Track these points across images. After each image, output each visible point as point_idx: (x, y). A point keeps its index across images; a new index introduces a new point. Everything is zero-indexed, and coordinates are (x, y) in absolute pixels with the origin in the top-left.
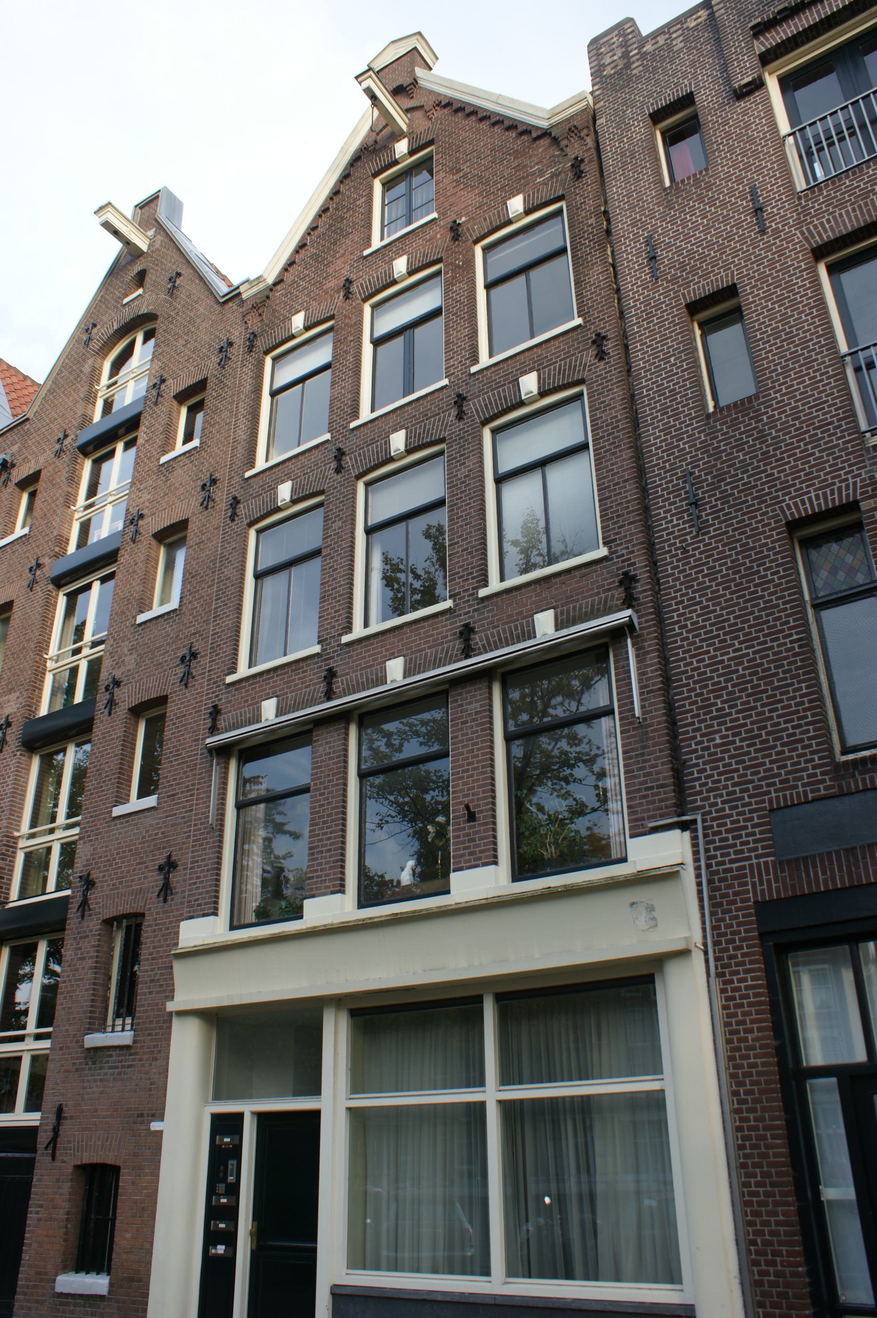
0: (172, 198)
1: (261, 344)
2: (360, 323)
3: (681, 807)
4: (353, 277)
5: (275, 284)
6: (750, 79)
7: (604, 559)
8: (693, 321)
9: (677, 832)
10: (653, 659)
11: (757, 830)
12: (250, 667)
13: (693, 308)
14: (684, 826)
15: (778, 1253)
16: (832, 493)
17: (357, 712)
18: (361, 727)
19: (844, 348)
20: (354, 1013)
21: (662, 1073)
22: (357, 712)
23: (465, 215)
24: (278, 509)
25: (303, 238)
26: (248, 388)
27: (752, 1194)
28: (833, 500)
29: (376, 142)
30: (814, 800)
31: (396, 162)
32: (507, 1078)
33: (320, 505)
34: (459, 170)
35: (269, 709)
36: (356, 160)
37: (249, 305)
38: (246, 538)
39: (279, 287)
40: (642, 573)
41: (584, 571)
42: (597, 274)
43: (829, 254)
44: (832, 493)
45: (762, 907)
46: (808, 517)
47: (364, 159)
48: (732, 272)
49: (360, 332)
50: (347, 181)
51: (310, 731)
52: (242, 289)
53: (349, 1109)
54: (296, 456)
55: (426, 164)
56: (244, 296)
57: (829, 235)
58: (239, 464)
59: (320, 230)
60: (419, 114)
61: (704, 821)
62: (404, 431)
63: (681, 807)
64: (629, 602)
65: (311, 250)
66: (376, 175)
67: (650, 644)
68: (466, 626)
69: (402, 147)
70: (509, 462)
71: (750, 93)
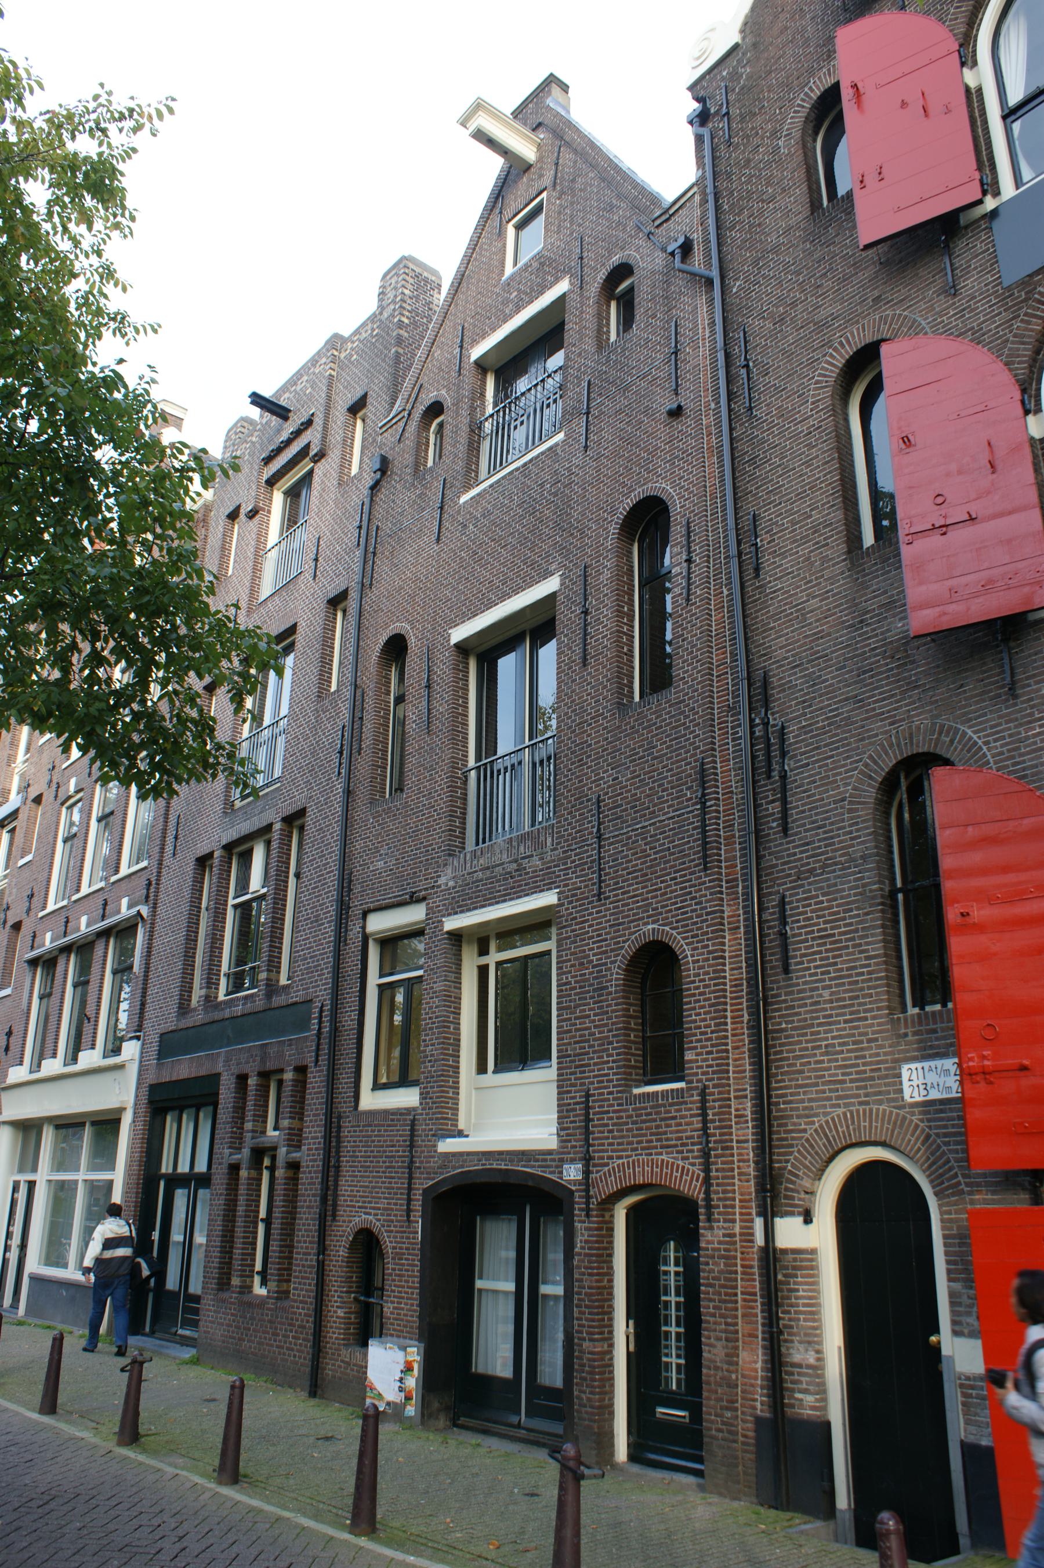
9: (135, 1041)
14: (138, 1038)
18: (116, 937)
22: (115, 930)
38: (59, 814)
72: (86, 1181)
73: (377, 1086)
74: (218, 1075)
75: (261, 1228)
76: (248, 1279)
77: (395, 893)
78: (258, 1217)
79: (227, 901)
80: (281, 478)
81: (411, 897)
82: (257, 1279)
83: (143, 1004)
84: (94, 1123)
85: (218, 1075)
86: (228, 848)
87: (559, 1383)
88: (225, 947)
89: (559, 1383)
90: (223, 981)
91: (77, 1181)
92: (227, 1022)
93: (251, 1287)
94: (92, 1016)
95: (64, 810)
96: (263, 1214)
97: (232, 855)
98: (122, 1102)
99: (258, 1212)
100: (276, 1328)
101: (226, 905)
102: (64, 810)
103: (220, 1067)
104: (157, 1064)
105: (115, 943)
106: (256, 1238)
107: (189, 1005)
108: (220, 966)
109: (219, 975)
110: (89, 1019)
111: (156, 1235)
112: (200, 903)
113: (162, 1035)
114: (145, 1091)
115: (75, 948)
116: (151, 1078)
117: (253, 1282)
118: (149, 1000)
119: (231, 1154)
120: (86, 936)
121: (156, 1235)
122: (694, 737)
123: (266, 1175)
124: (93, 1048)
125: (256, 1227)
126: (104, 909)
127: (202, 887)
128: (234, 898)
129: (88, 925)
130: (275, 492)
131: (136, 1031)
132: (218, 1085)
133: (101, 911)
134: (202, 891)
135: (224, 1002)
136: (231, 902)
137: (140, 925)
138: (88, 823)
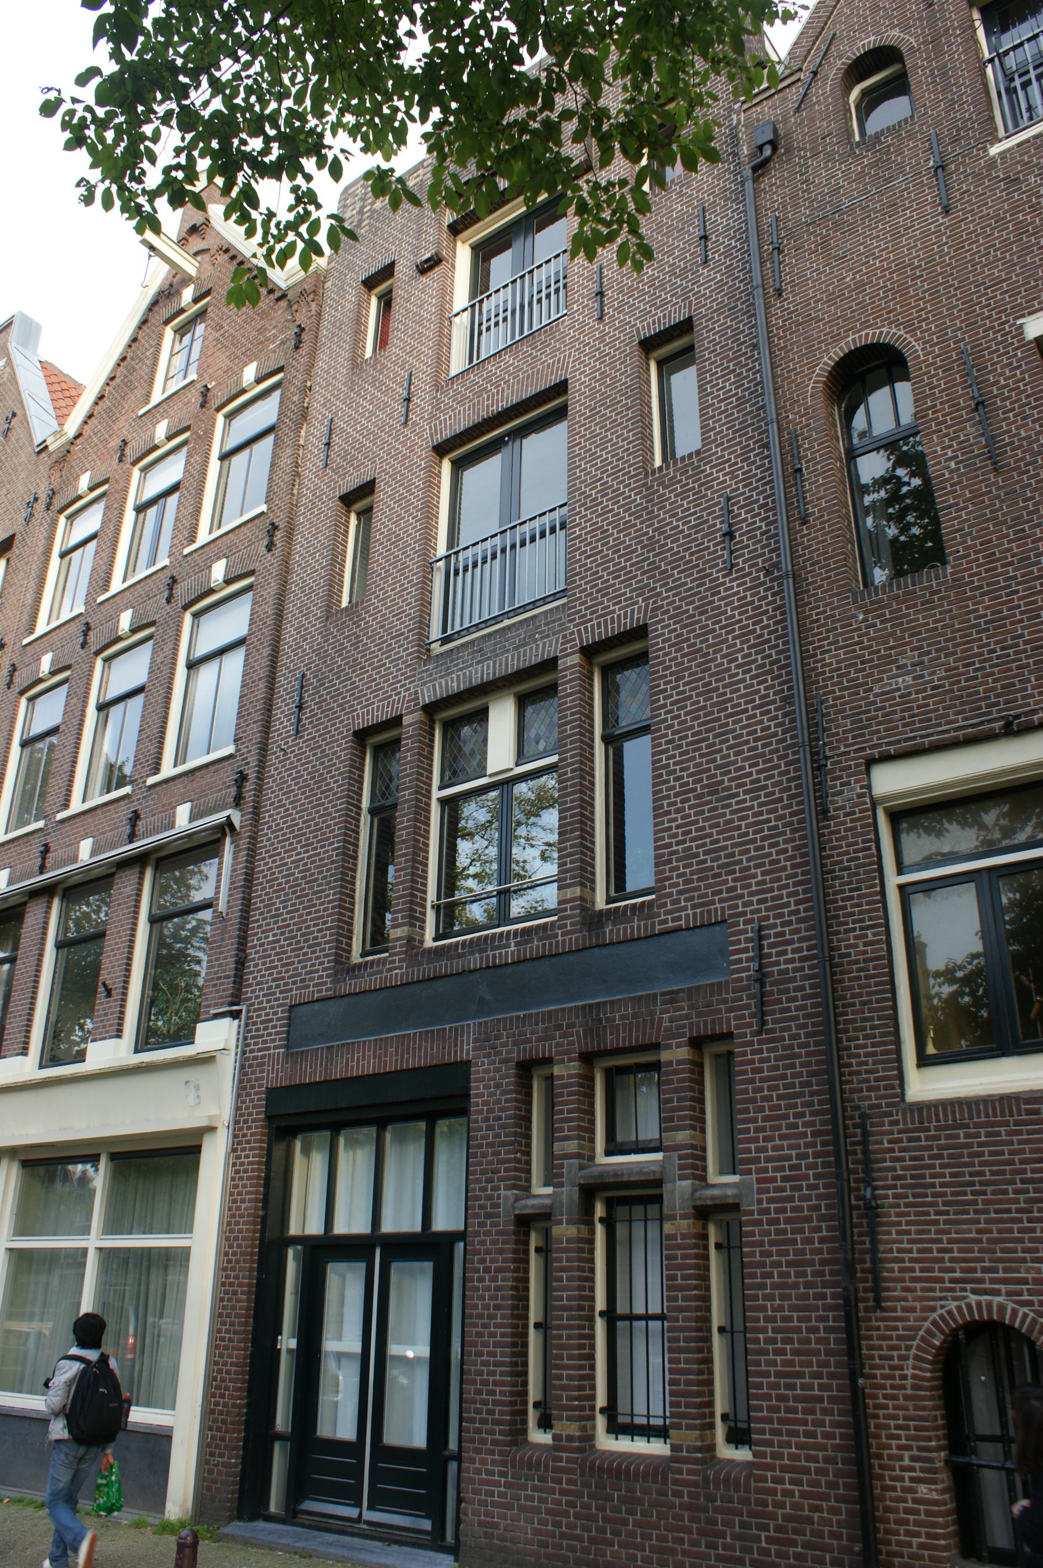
0: (28, 322)
1: (58, 502)
2: (126, 489)
3: (236, 998)
4: (129, 437)
5: (76, 438)
6: (428, 255)
7: (231, 756)
8: (349, 512)
9: (227, 1021)
10: (243, 857)
11: (801, 907)
12: (175, 766)
13: (648, 345)
14: (235, 1015)
15: (227, 1388)
16: (613, 622)
17: (155, 856)
18: (156, 868)
19: (442, 550)
20: (25, 1164)
21: (191, 1232)
22: (155, 856)
23: (216, 379)
24: (119, 639)
25: (103, 389)
26: (41, 549)
27: (222, 1339)
28: (600, 634)
29: (171, 285)
30: (318, 1000)
31: (182, 311)
32: (112, 1227)
33: (249, 588)
34: (222, 327)
35: (183, 813)
36: (155, 304)
37: (54, 457)
38: (16, 707)
39: (78, 441)
40: (251, 773)
41: (217, 766)
42: (286, 462)
43: (452, 450)
44: (613, 622)
45: (272, 1093)
46: (602, 642)
47: (161, 304)
48: (690, 303)
49: (124, 499)
50: (144, 328)
51: (113, 875)
52: (48, 443)
53: (10, 1250)
54: (239, 526)
55: (202, 315)
56: (51, 449)
57: (447, 434)
58: (22, 629)
59: (117, 380)
60: (207, 257)
61: (248, 1011)
62: (224, 561)
63: (236, 998)
64: (238, 801)
65: (106, 403)
66: (167, 322)
67: (244, 843)
68: (135, 812)
69: (188, 294)
70: (207, 644)
71: (431, 268)
72: (100, 1249)
73: (924, 1061)
74: (463, 1067)
75: (600, 1327)
76: (589, 1423)
77: (958, 722)
78: (592, 1308)
79: (429, 792)
80: (471, 225)
81: (1008, 725)
82: (601, 1422)
83: (241, 963)
84: (113, 1157)
85: (463, 1067)
86: (431, 710)
87: (419, 1440)
88: (358, 883)
89: (419, 1440)
90: (430, 917)
91: (85, 1251)
92: (477, 975)
93: (591, 1438)
94: (116, 986)
95: (23, 702)
96: (600, 1304)
97: (364, 747)
98: (210, 1117)
99: (592, 1299)
100: (713, 1522)
101: (430, 798)
102: (23, 702)
103: (466, 1049)
104: (287, 1055)
105: (155, 878)
106: (593, 1347)
107: (348, 958)
108: (425, 892)
109: (424, 907)
110: (109, 993)
111: (288, 1342)
112: (360, 801)
113: (291, 1006)
114: (257, 1100)
115: (60, 889)
116: (275, 1075)
117: (594, 1428)
118: (252, 954)
119: (517, 1199)
120: (87, 869)
121: (288, 1342)
122: (673, 719)
123: (600, 1231)
124: (119, 1037)
125: (592, 1328)
126: (44, 859)
127: (362, 777)
128: (440, 788)
129: (93, 853)
130: (459, 244)
131: (232, 1004)
132: (467, 1079)
133: (233, 791)
134: (361, 783)
135: (430, 951)
136: (436, 794)
137: (228, 840)
138: (83, 711)
